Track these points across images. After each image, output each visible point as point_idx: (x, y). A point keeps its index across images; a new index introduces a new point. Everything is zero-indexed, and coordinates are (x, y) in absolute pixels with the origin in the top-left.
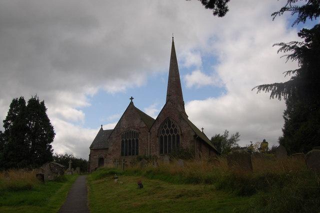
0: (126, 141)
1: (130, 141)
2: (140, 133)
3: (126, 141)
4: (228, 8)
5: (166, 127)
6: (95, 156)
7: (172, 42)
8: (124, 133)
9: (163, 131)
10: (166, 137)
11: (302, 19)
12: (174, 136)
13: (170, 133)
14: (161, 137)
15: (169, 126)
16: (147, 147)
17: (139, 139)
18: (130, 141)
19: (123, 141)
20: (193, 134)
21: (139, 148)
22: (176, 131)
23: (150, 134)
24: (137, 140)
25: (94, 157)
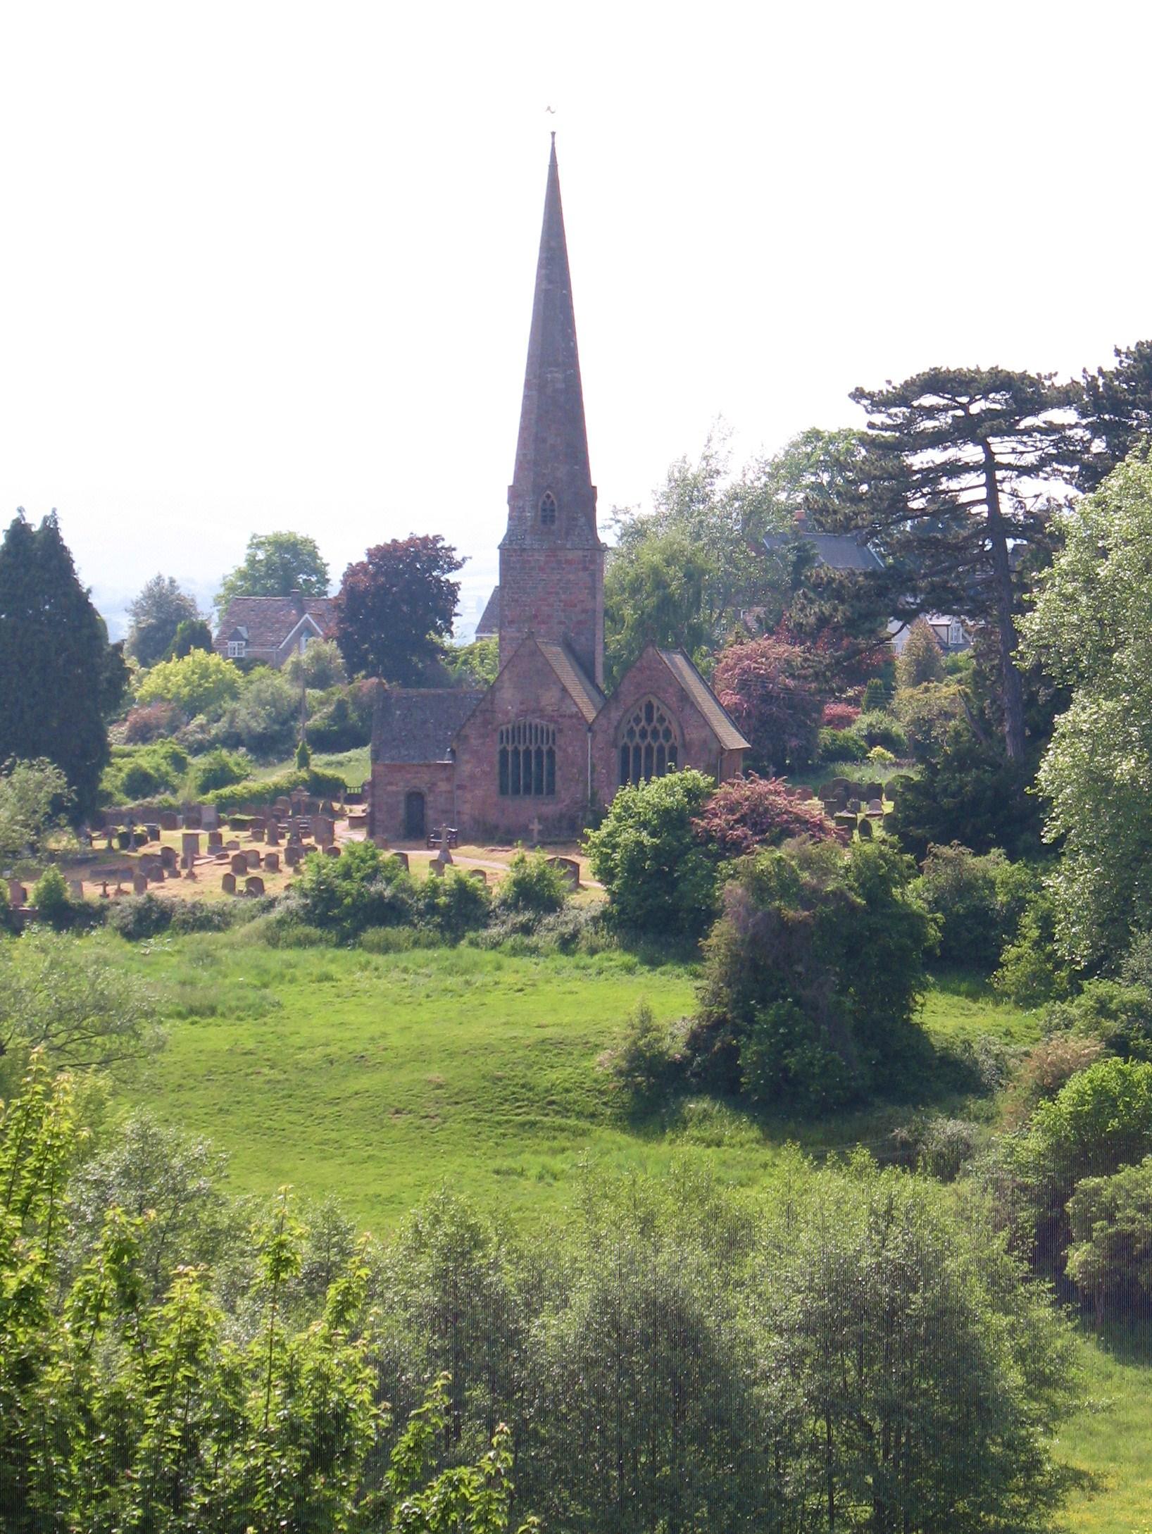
0: (516, 752)
1: (527, 753)
2: (560, 731)
3: (516, 752)
4: (853, 390)
5: (637, 720)
6: (391, 784)
7: (544, 1022)
8: (510, 726)
9: (631, 732)
10: (649, 749)
11: (541, 793)
12: (637, 749)
13: (662, 740)
14: (625, 750)
15: (649, 719)
16: (593, 766)
17: (555, 748)
18: (527, 753)
19: (504, 753)
20: (714, 746)
21: (558, 773)
22: (667, 733)
23: (594, 738)
24: (551, 753)
25: (389, 788)
